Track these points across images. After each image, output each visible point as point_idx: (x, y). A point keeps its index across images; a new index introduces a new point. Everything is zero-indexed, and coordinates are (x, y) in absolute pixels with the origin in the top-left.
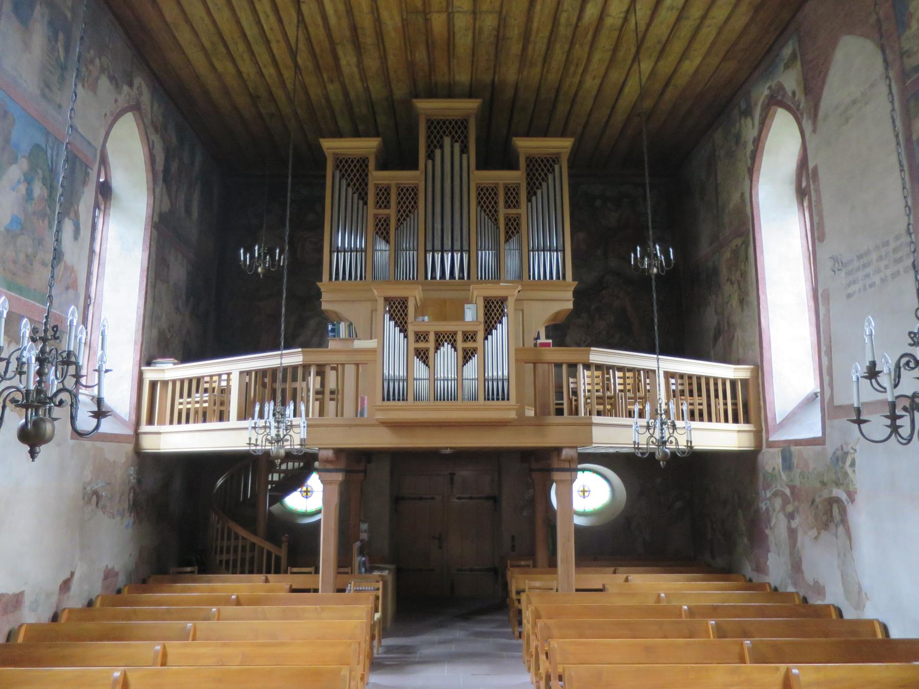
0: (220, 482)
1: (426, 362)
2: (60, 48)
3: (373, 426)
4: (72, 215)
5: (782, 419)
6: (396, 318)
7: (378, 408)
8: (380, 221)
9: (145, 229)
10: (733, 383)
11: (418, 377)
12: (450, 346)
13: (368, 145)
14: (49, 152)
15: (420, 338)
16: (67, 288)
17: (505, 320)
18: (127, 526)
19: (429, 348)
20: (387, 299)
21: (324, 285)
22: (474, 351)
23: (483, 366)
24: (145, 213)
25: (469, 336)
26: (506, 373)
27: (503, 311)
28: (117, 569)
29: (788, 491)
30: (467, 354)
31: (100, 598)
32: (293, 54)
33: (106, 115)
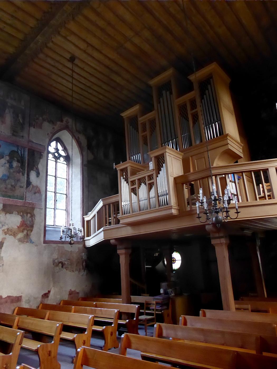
2: (20, 119)
4: (35, 169)
9: (81, 167)
13: (135, 109)
14: (19, 152)
16: (35, 193)
18: (82, 275)
24: (80, 162)
28: (77, 291)
31: (62, 301)
32: (100, 87)
33: (48, 134)
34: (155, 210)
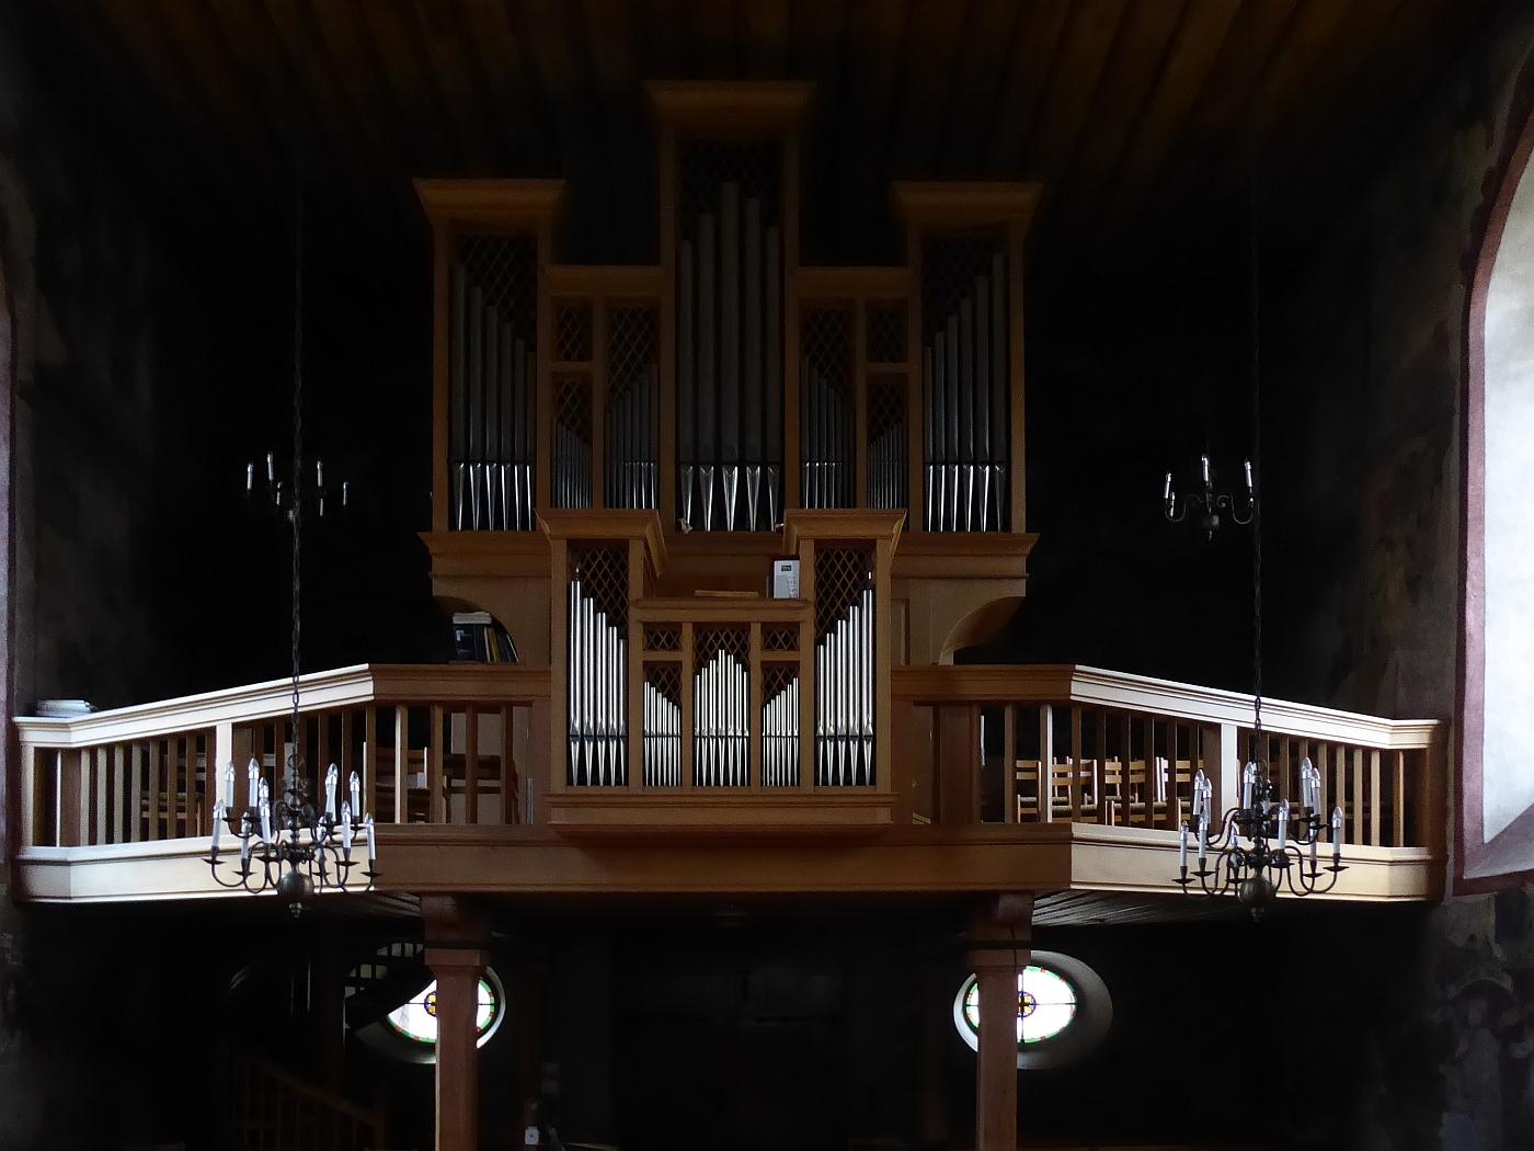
0: (237, 980)
1: (673, 695)
3: (546, 844)
5: (1497, 833)
6: (600, 593)
7: (554, 800)
8: (568, 390)
10: (1388, 756)
11: (654, 731)
12: (731, 659)
15: (658, 639)
17: (867, 596)
19: (680, 663)
20: (576, 546)
21: (436, 539)
22: (789, 672)
23: (810, 710)
25: (781, 634)
26: (867, 719)
27: (863, 576)
29: (1507, 983)
30: (775, 677)
34: (714, 796)
